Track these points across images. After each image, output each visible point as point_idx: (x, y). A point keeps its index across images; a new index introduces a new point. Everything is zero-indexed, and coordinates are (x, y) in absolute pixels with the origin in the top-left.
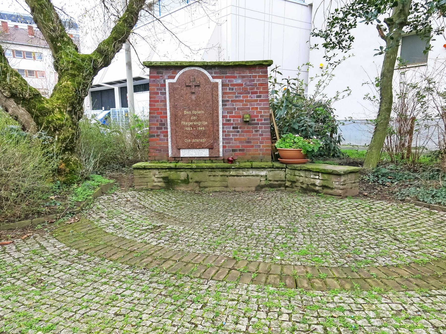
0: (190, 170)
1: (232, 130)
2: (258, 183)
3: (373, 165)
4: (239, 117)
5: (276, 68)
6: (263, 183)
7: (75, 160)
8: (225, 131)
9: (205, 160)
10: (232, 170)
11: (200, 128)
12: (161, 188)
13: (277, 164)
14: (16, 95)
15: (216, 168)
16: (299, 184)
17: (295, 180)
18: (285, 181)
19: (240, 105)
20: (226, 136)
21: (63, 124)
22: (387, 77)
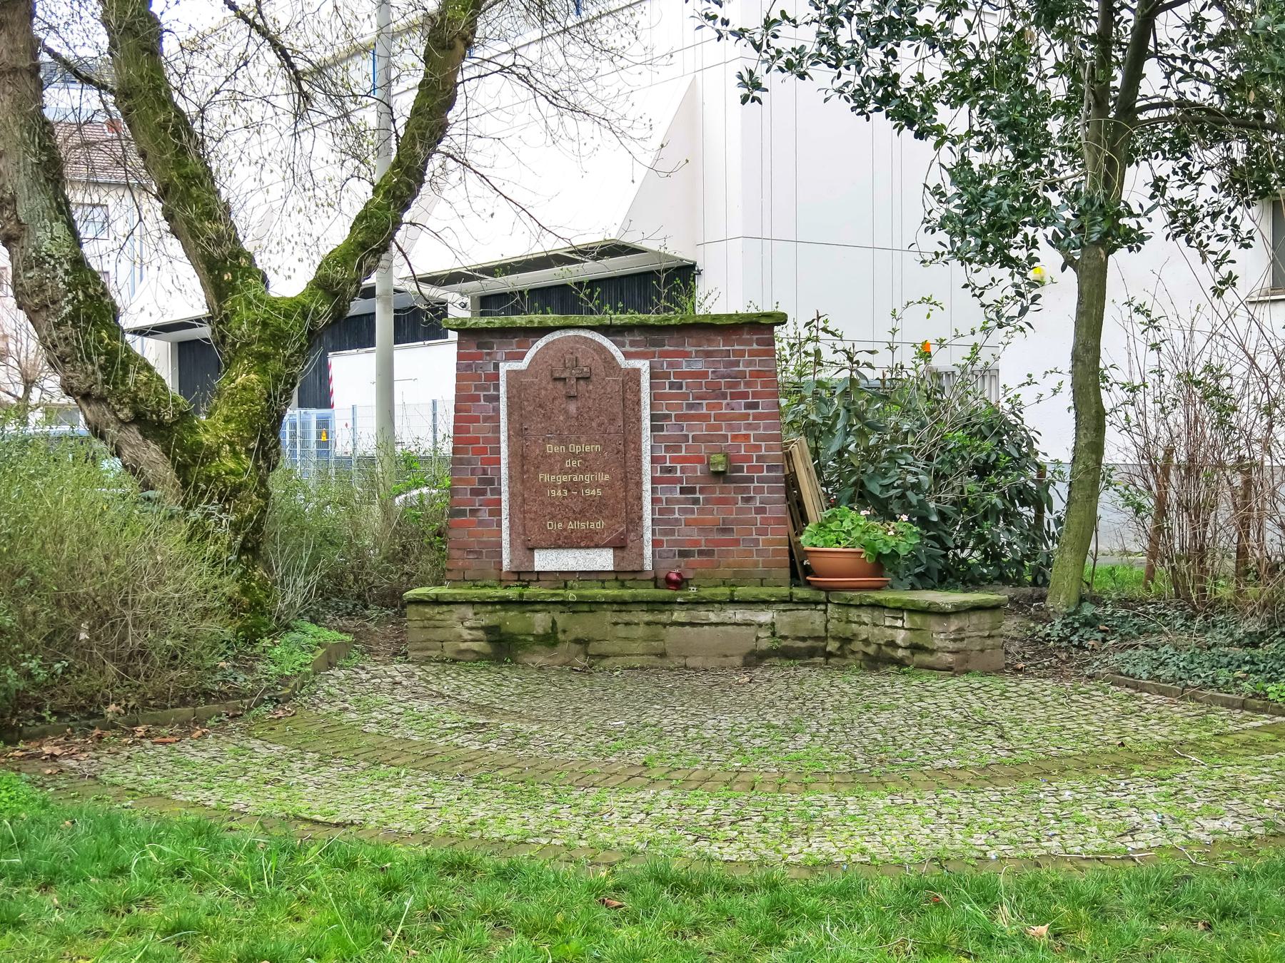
0: (560, 607)
1: (678, 495)
2: (751, 644)
3: (1067, 596)
4: (700, 460)
5: (819, 318)
6: (765, 644)
7: (262, 577)
8: (659, 500)
9: (603, 582)
10: (677, 607)
11: (588, 492)
12: (480, 656)
13: (802, 593)
14: (145, 415)
15: (634, 602)
16: (858, 646)
17: (848, 635)
18: (825, 639)
19: (701, 429)
20: (661, 512)
21: (241, 484)
22: (1083, 363)
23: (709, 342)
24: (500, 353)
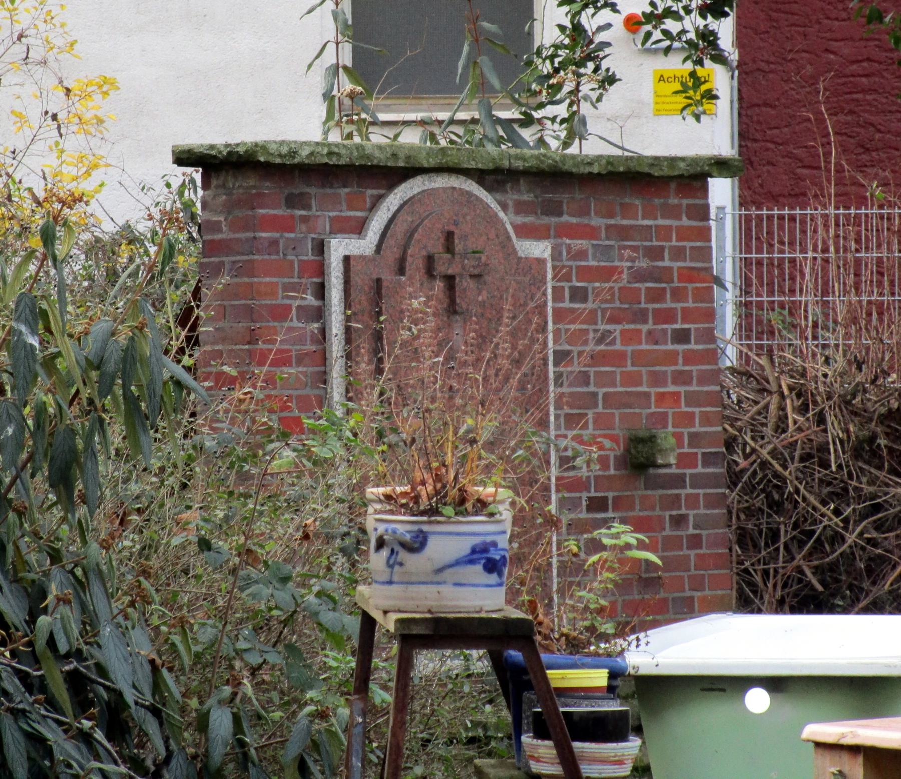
23: (626, 210)
24: (324, 217)
